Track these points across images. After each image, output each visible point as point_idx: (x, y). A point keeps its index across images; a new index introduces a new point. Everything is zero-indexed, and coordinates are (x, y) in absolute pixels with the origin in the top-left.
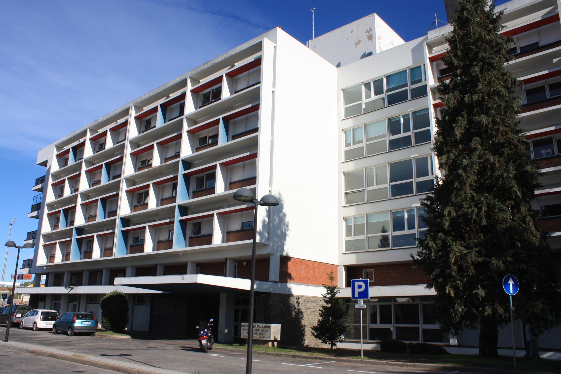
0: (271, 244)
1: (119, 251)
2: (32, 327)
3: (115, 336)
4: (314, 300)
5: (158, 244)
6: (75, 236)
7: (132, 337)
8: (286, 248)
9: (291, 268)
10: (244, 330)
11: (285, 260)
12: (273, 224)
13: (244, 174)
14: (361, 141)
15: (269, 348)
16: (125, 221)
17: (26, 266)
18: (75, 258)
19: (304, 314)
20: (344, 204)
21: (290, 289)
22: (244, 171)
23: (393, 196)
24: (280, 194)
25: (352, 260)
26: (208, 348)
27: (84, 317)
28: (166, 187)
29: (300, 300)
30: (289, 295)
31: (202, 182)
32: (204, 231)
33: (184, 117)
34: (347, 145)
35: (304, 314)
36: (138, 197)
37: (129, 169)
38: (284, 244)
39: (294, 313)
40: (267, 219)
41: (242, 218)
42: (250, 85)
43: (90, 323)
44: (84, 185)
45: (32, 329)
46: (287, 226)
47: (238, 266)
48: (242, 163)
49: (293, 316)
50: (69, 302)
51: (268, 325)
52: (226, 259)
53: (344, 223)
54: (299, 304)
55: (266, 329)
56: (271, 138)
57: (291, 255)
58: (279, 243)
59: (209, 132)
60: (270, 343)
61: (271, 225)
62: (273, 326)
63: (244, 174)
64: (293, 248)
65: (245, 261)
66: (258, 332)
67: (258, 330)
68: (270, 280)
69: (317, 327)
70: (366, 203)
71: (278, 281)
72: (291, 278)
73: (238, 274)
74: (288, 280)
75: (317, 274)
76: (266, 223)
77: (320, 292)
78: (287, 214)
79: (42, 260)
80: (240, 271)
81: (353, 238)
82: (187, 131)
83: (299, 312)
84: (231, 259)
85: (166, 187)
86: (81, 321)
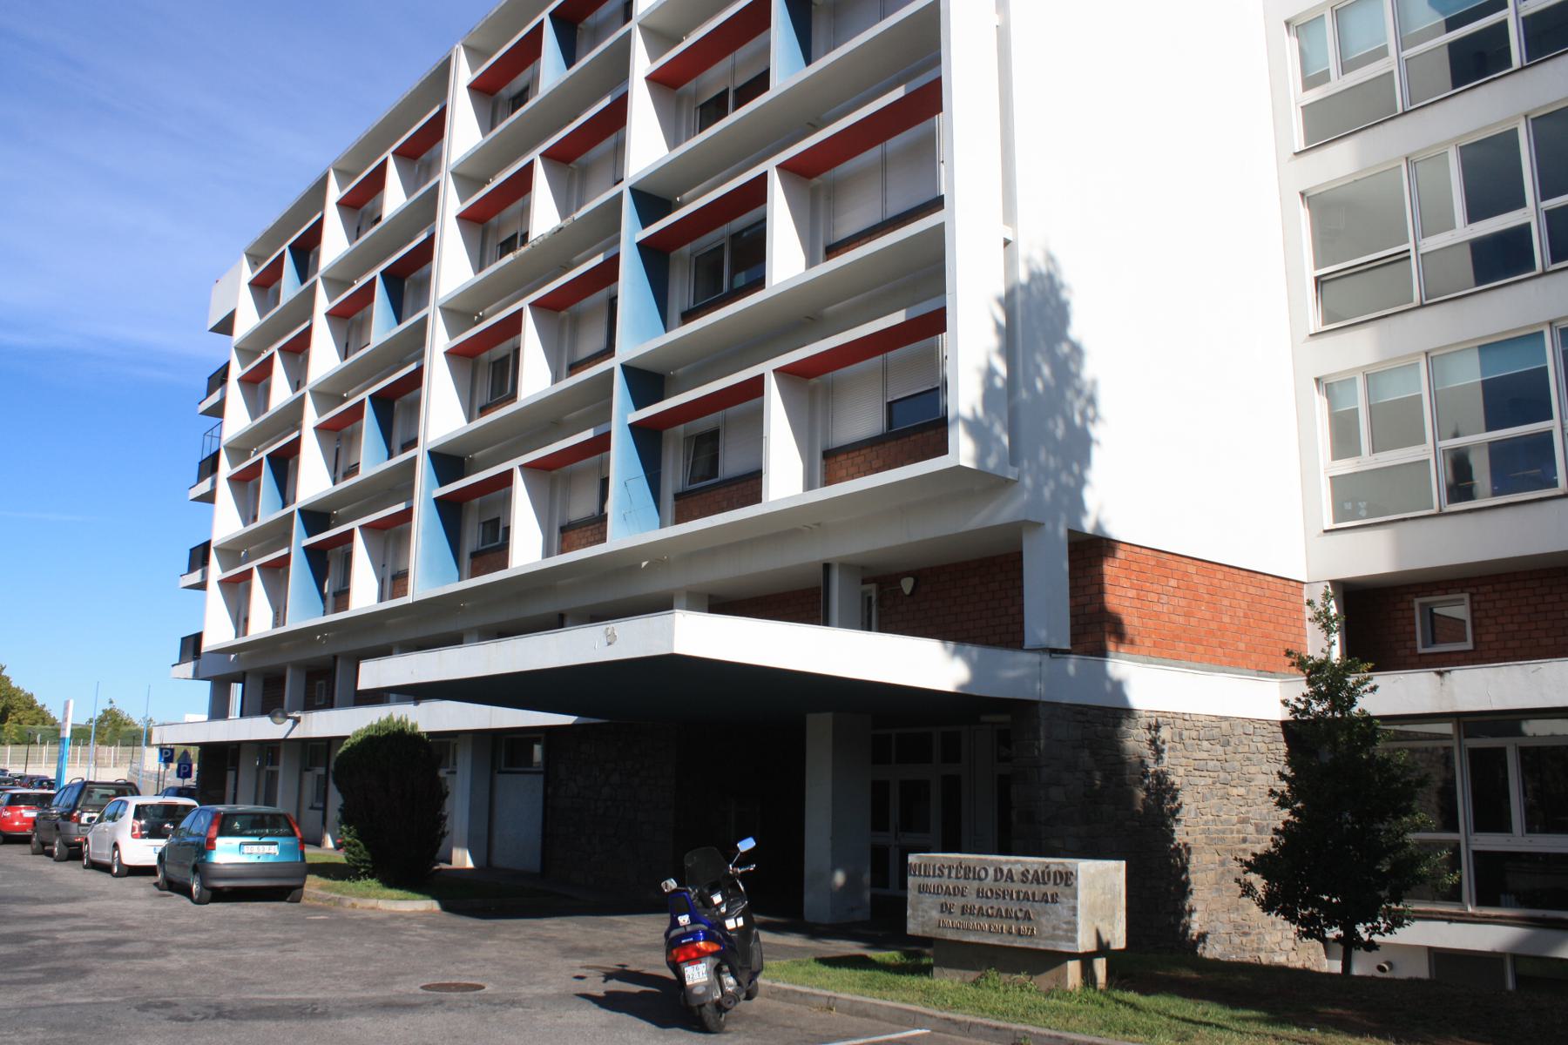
0: (1028, 481)
1: (430, 572)
2: (108, 860)
3: (372, 903)
4: (1223, 732)
5: (564, 533)
6: (300, 539)
7: (445, 908)
8: (1090, 497)
9: (1120, 592)
10: (922, 889)
11: (1090, 552)
12: (1031, 387)
13: (885, 201)
14: (1382, 53)
15: (1066, 994)
16: (448, 462)
17: (190, 654)
18: (305, 612)
19: (1184, 797)
20: (1315, 322)
21: (1118, 686)
22: (884, 189)
23: (1554, 261)
24: (1050, 258)
25: (1372, 555)
26: (720, 1007)
27: (257, 826)
28: (578, 305)
29: (1165, 733)
30: (1122, 713)
31: (708, 252)
32: (730, 465)
33: (633, 25)
34: (1311, 81)
35: (1181, 797)
36: (487, 365)
37: (453, 269)
38: (1081, 482)
39: (1141, 794)
40: (1001, 367)
41: (885, 385)
42: (895, 209)
43: (274, 849)
44: (325, 358)
45: (105, 868)
46: (1091, 401)
47: (880, 599)
48: (873, 154)
49: (1139, 807)
50: (305, 768)
51: (1055, 863)
52: (827, 567)
53: (1320, 404)
54: (1159, 752)
55: (1050, 889)
56: (996, 20)
57: (1115, 531)
58: (1064, 478)
59: (734, 70)
60: (1074, 967)
61: (1024, 394)
62: (1086, 869)
63: (885, 201)
64: (1117, 501)
65: (907, 574)
66: (1002, 905)
67: (1001, 895)
68: (1028, 643)
69: (1268, 854)
70: (1422, 306)
71: (1067, 646)
72: (1120, 636)
73: (880, 616)
74: (1111, 645)
75: (1226, 619)
76: (999, 383)
77: (1267, 699)
78: (1087, 345)
79: (219, 632)
80: (892, 602)
81: (1367, 460)
82: (649, 79)
83: (1164, 791)
84: (848, 567)
85: (578, 305)
86: (236, 841)
